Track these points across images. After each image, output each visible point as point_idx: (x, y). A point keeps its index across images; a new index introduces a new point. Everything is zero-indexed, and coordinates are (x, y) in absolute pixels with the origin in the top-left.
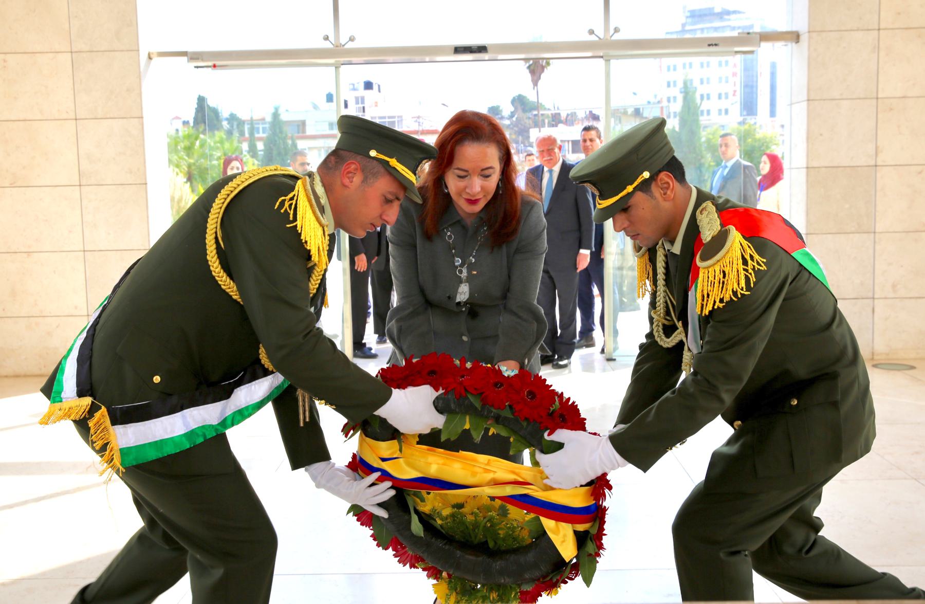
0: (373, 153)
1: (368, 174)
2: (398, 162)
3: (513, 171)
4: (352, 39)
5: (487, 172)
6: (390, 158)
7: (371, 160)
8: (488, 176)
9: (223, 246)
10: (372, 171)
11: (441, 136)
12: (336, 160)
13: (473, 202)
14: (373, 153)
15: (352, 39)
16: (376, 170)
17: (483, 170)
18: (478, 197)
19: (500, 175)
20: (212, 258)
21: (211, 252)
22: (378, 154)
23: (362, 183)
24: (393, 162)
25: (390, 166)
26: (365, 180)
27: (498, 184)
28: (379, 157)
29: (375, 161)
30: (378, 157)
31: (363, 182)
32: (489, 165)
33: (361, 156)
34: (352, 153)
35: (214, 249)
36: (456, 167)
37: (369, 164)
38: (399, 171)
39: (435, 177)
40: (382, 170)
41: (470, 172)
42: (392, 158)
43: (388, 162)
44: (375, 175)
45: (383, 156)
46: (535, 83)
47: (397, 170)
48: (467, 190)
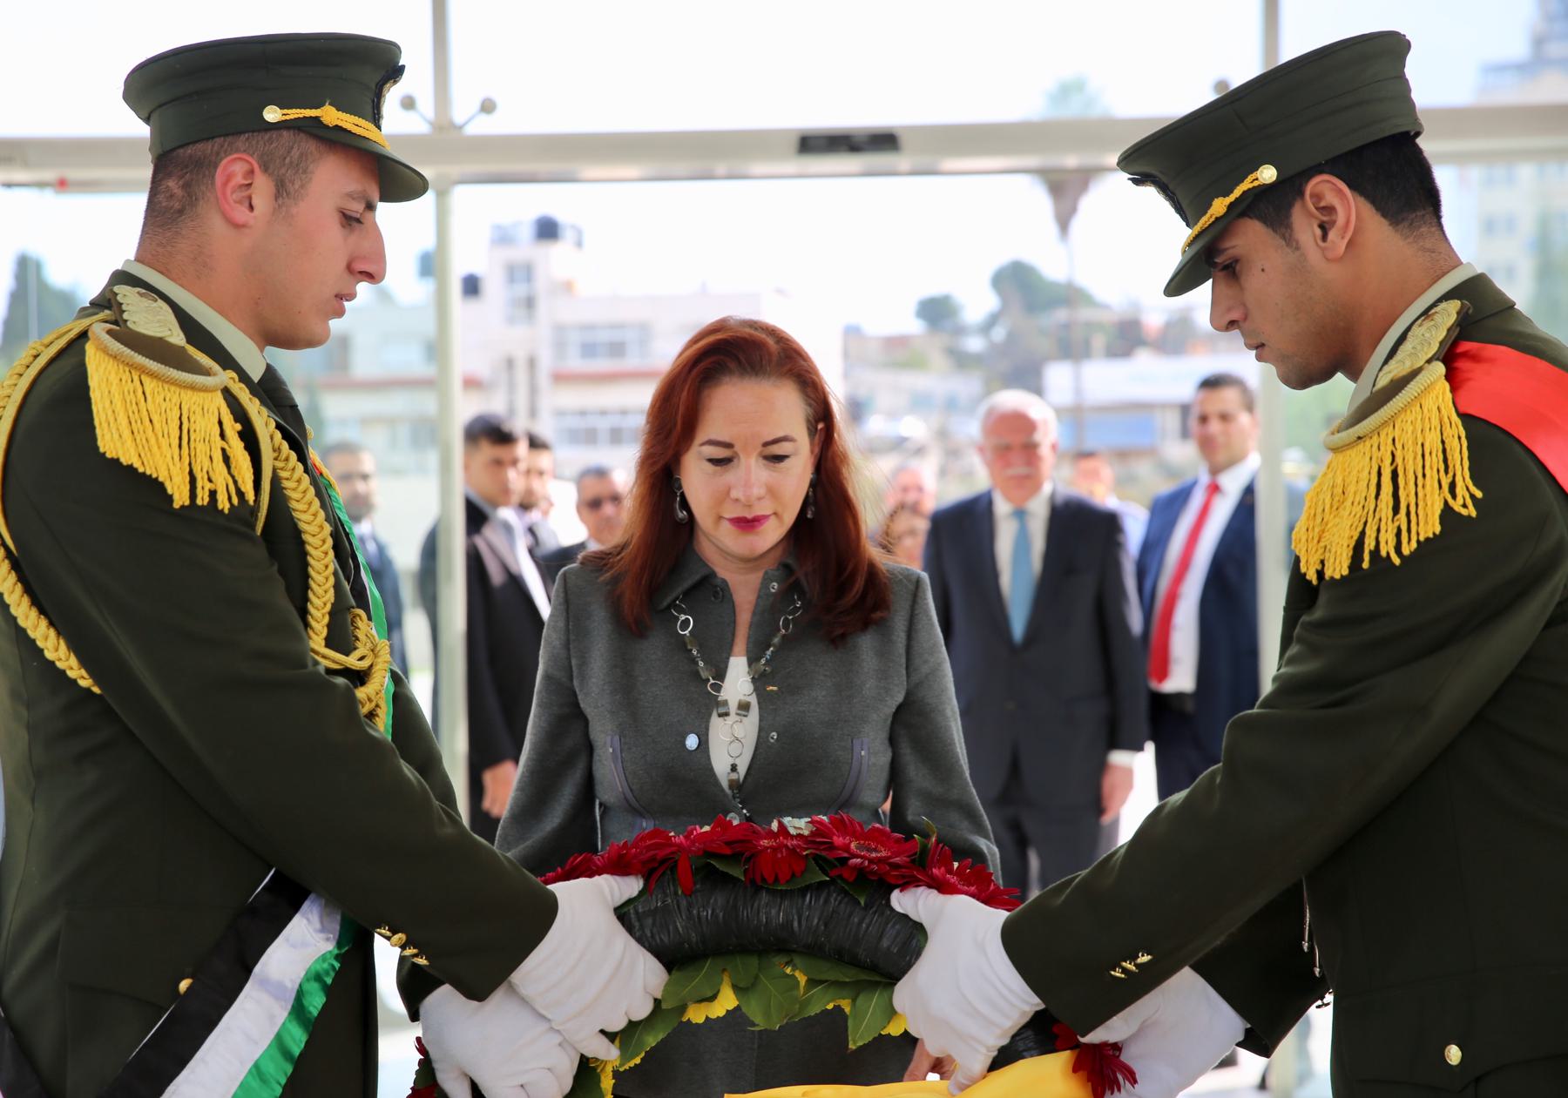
0: (272, 114)
1: (283, 171)
2: (338, 110)
3: (842, 461)
4: (488, 107)
5: (777, 450)
6: (316, 108)
7: (274, 134)
8: (779, 458)
9: (85, 682)
10: (288, 160)
11: (681, 358)
12: (181, 183)
13: (748, 524)
14: (272, 114)
15: (488, 107)
16: (295, 153)
17: (766, 444)
18: (759, 510)
19: (812, 474)
20: (57, 650)
21: (27, 617)
22: (286, 111)
23: (276, 198)
24: (330, 115)
25: (327, 127)
26: (281, 190)
27: (808, 493)
28: (292, 117)
29: (285, 133)
30: (287, 118)
31: (278, 196)
32: (781, 434)
33: (243, 137)
34: (219, 141)
35: (9, 572)
36: (706, 439)
37: (274, 145)
38: (350, 132)
39: (655, 468)
40: (311, 146)
41: (737, 448)
42: (323, 105)
43: (317, 119)
44: (301, 167)
45: (298, 111)
46: (1064, 221)
47: (345, 130)
48: (734, 494)
